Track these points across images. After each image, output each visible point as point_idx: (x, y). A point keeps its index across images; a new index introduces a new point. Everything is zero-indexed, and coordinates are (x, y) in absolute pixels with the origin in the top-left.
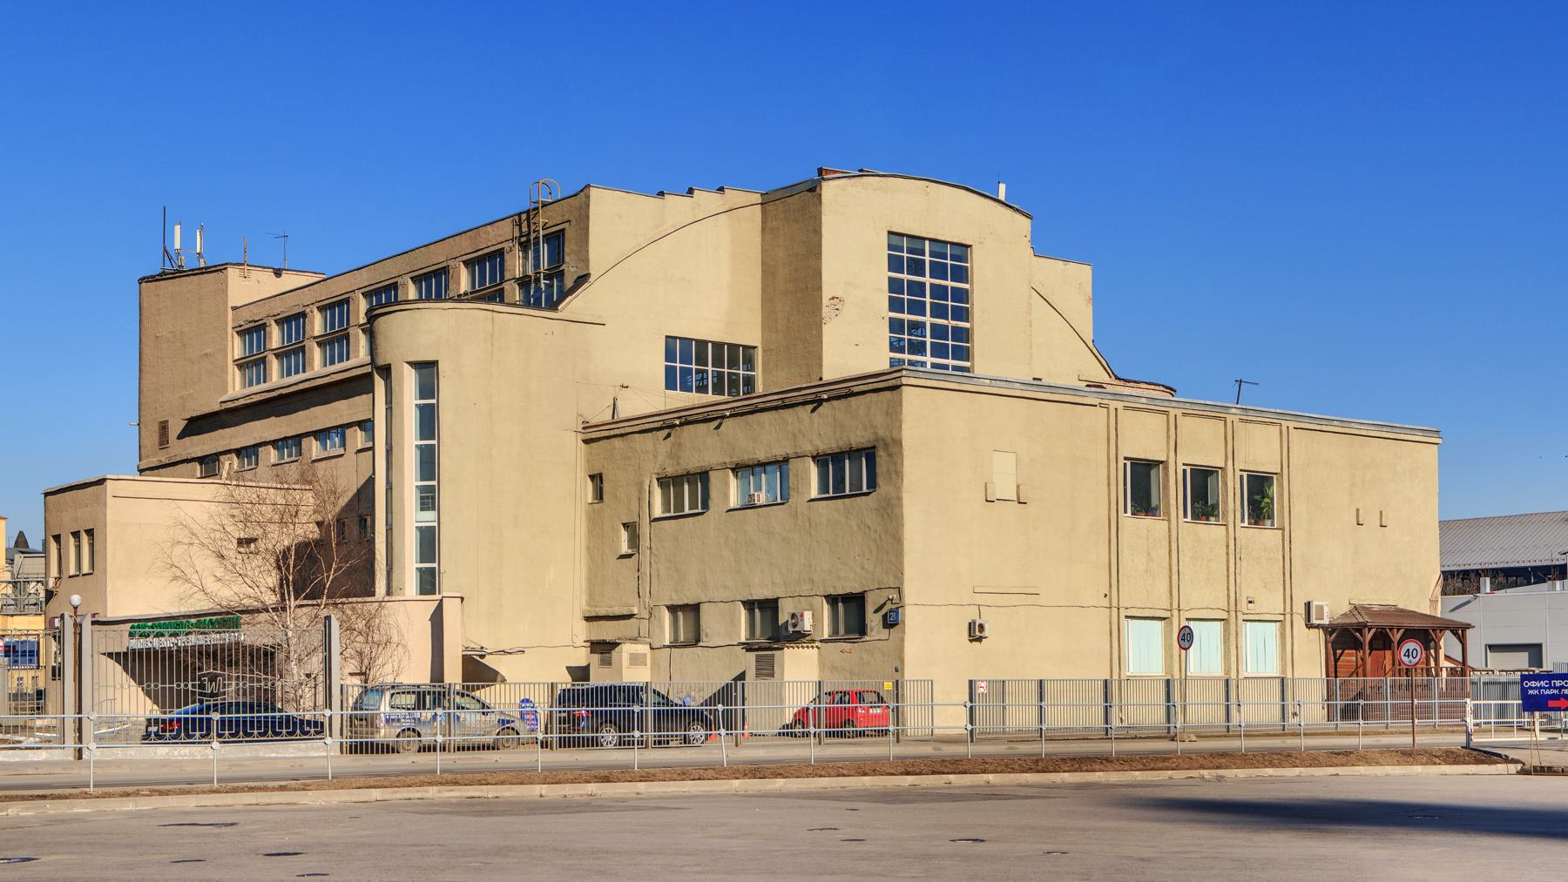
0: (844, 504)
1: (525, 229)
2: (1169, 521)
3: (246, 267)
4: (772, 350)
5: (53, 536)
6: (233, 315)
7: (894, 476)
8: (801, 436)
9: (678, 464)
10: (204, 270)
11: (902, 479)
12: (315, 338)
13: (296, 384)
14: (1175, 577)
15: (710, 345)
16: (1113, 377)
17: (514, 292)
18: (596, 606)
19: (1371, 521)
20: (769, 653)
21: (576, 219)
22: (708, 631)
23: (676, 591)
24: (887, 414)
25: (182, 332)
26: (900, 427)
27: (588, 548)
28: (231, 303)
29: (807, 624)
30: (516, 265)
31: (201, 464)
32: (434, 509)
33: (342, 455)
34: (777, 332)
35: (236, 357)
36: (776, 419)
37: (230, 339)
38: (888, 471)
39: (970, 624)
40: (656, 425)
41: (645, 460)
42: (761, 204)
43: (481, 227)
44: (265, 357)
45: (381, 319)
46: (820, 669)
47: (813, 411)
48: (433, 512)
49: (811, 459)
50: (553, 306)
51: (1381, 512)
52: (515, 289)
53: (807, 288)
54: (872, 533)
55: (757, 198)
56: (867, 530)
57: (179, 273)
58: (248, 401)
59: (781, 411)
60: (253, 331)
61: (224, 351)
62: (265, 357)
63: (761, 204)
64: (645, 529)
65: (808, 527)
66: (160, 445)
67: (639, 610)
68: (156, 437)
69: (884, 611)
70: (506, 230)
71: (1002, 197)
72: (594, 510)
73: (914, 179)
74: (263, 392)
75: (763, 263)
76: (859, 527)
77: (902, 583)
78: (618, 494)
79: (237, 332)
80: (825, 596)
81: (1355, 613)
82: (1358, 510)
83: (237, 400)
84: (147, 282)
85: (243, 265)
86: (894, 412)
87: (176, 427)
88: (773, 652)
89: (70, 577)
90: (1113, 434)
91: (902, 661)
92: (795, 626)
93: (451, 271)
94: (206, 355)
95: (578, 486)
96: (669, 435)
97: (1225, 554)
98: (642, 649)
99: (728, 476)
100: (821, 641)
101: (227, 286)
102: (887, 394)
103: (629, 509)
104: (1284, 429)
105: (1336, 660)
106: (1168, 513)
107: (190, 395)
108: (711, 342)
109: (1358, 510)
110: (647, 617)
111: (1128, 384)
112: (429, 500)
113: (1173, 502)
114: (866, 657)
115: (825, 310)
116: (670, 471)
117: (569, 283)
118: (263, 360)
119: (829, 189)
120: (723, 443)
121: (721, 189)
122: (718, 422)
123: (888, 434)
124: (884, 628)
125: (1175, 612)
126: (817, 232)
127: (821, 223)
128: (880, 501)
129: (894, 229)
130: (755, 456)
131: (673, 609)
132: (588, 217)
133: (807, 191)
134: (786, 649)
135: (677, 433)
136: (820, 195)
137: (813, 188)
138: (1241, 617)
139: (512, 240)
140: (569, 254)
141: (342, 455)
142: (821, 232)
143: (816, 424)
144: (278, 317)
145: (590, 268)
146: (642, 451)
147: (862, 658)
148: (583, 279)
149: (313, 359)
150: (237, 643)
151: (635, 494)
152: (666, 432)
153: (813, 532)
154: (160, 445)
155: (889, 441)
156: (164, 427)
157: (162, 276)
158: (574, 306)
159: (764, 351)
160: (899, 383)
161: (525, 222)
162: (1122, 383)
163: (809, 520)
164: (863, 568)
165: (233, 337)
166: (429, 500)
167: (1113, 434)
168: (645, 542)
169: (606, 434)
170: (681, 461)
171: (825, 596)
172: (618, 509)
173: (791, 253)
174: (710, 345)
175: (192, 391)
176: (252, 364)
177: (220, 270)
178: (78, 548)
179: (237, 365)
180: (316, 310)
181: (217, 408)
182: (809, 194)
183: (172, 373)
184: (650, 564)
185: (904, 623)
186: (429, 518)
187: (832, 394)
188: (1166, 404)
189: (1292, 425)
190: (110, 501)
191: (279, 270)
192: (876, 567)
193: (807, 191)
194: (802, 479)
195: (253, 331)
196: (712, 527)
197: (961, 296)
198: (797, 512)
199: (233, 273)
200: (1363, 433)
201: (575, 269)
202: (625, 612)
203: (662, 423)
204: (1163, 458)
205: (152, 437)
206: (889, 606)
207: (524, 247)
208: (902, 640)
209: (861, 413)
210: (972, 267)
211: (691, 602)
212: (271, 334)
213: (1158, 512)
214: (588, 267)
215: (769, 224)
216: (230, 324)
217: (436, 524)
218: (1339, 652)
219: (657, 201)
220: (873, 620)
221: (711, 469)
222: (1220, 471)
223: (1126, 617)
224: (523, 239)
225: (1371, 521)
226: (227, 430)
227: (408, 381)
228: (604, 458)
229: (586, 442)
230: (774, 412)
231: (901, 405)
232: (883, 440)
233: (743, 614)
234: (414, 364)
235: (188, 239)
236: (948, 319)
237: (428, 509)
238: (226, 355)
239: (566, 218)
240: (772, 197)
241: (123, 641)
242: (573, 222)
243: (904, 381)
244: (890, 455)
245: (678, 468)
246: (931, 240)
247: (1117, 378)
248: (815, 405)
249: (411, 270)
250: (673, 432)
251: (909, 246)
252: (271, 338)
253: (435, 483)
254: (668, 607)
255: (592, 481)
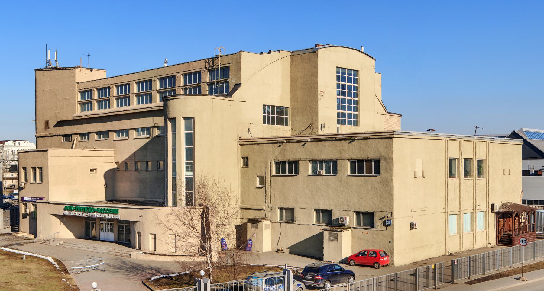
0: (365, 178)
1: (211, 64)
2: (460, 179)
3: (82, 68)
4: (295, 109)
5: (23, 168)
6: (77, 85)
7: (389, 171)
8: (344, 152)
9: (284, 157)
10: (65, 69)
11: (393, 172)
12: (114, 96)
13: (108, 113)
14: (461, 199)
15: (275, 107)
16: (387, 112)
17: (205, 88)
18: (245, 204)
19: (507, 173)
20: (335, 232)
21: (235, 63)
22: (298, 218)
23: (283, 203)
24: (386, 148)
25: (55, 90)
26: (393, 153)
27: (241, 183)
28: (76, 81)
29: (347, 222)
30: (206, 77)
31: (63, 137)
32: (192, 171)
33: (127, 140)
34: (298, 102)
35: (79, 101)
36: (331, 145)
37: (76, 94)
38: (386, 169)
39: (411, 224)
40: (274, 142)
41: (268, 154)
42: (291, 56)
43: (190, 62)
44: (92, 101)
45: (171, 101)
46: (352, 238)
47: (350, 143)
48: (192, 172)
49: (348, 161)
50: (230, 94)
51: (509, 170)
52: (206, 86)
53: (311, 88)
54: (378, 191)
55: (289, 54)
56: (376, 190)
57: (51, 69)
58: (86, 117)
59: (334, 142)
60: (86, 92)
61: (74, 98)
62: (92, 101)
63: (291, 56)
64: (268, 179)
65: (347, 186)
66: (46, 129)
67: (266, 208)
68: (44, 126)
69: (384, 220)
70: (202, 64)
71: (363, 50)
72: (244, 170)
73: (344, 47)
74: (93, 115)
75: (291, 77)
76: (372, 188)
77: (393, 210)
78: (256, 165)
79: (79, 92)
80: (355, 212)
81: (503, 205)
82: (504, 170)
83: (81, 116)
84: (39, 71)
85: (80, 67)
86: (390, 147)
87: (52, 123)
88: (337, 232)
89: (31, 183)
90: (446, 151)
91: (393, 239)
92: (342, 222)
93: (176, 77)
94: (66, 99)
95: (238, 161)
96: (280, 146)
97: (472, 189)
98: (268, 222)
99: (308, 163)
100: (353, 228)
101: (75, 75)
102: (386, 140)
103: (261, 171)
104: (487, 143)
105: (499, 223)
106: (459, 177)
107: (59, 112)
108: (276, 106)
109: (504, 170)
110: (269, 211)
111: (391, 115)
112: (190, 167)
113: (461, 173)
114: (375, 236)
115: (319, 96)
116: (281, 159)
117: (232, 87)
118: (91, 103)
119: (321, 52)
120: (306, 151)
121: (279, 51)
122: (304, 143)
123: (386, 155)
124: (383, 226)
125: (461, 212)
126: (316, 67)
127: (318, 64)
128: (382, 180)
129: (338, 66)
130: (321, 157)
131: (281, 209)
132: (240, 63)
133: (312, 52)
134: (343, 232)
135: (283, 145)
136: (317, 54)
137: (314, 51)
138: (477, 211)
139: (205, 68)
140: (231, 75)
141: (127, 140)
142: (318, 68)
143: (351, 148)
144: (97, 88)
145: (241, 81)
146: (267, 151)
147: (373, 236)
148: (237, 86)
149: (113, 104)
150: (271, 286)
151: (263, 166)
152: (279, 144)
153: (349, 188)
154: (46, 129)
155: (387, 157)
156: (47, 123)
157: (46, 69)
158: (236, 95)
159: (292, 109)
160: (392, 137)
161: (211, 62)
162: (389, 114)
163: (348, 183)
164: (373, 203)
165: (77, 93)
166: (190, 167)
167: (446, 151)
168: (268, 183)
169: (251, 143)
170: (286, 156)
171: (355, 212)
172: (255, 169)
173: (304, 74)
174: (275, 107)
175: (59, 111)
176: (86, 104)
177: (72, 69)
178: (35, 174)
179: (79, 103)
180: (114, 87)
181: (72, 119)
182: (313, 53)
183: (50, 104)
184: (271, 191)
185: (393, 225)
186: (190, 174)
187: (359, 138)
188: (459, 137)
189: (490, 141)
190: (49, 158)
191: (92, 69)
192: (380, 203)
193: (312, 52)
194: (344, 168)
195: (86, 92)
196: (300, 181)
197: (356, 88)
198: (341, 179)
199: (77, 70)
200: (506, 143)
201: (234, 81)
202: (259, 208)
203: (277, 141)
204: (458, 157)
205: (42, 126)
206: (386, 219)
207: (210, 71)
208: (393, 231)
209: (373, 146)
210: (359, 78)
211: (290, 207)
212: (94, 93)
213: (455, 176)
214: (240, 81)
215: (294, 63)
216: (76, 89)
217: (193, 177)
218: (499, 220)
219: (260, 56)
220: (378, 223)
221: (300, 160)
222: (471, 160)
223: (450, 215)
224: (210, 68)
225: (507, 173)
226: (75, 126)
227: (182, 125)
228: (249, 152)
229: (240, 145)
230: (330, 142)
231: (393, 145)
232: (384, 157)
233: (314, 213)
234: (185, 118)
235: (52, 55)
236: (352, 97)
237: (189, 171)
238: (75, 100)
239: (230, 62)
240: (296, 53)
241: (61, 211)
242: (234, 64)
243: (395, 136)
244: (388, 163)
245: (284, 158)
246: (348, 69)
247: (388, 113)
248: (350, 141)
249: (158, 75)
250: (282, 145)
251: (342, 71)
252: (94, 95)
253: (192, 162)
254: (279, 208)
255: (243, 159)
